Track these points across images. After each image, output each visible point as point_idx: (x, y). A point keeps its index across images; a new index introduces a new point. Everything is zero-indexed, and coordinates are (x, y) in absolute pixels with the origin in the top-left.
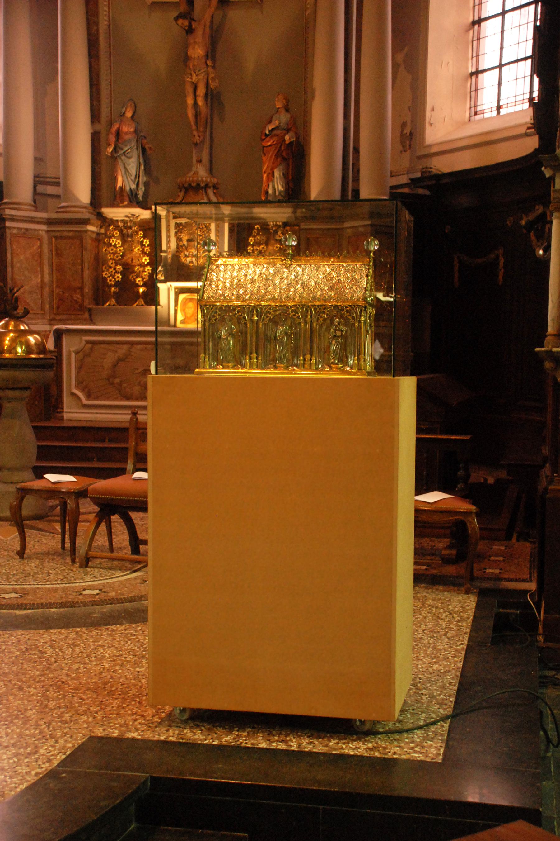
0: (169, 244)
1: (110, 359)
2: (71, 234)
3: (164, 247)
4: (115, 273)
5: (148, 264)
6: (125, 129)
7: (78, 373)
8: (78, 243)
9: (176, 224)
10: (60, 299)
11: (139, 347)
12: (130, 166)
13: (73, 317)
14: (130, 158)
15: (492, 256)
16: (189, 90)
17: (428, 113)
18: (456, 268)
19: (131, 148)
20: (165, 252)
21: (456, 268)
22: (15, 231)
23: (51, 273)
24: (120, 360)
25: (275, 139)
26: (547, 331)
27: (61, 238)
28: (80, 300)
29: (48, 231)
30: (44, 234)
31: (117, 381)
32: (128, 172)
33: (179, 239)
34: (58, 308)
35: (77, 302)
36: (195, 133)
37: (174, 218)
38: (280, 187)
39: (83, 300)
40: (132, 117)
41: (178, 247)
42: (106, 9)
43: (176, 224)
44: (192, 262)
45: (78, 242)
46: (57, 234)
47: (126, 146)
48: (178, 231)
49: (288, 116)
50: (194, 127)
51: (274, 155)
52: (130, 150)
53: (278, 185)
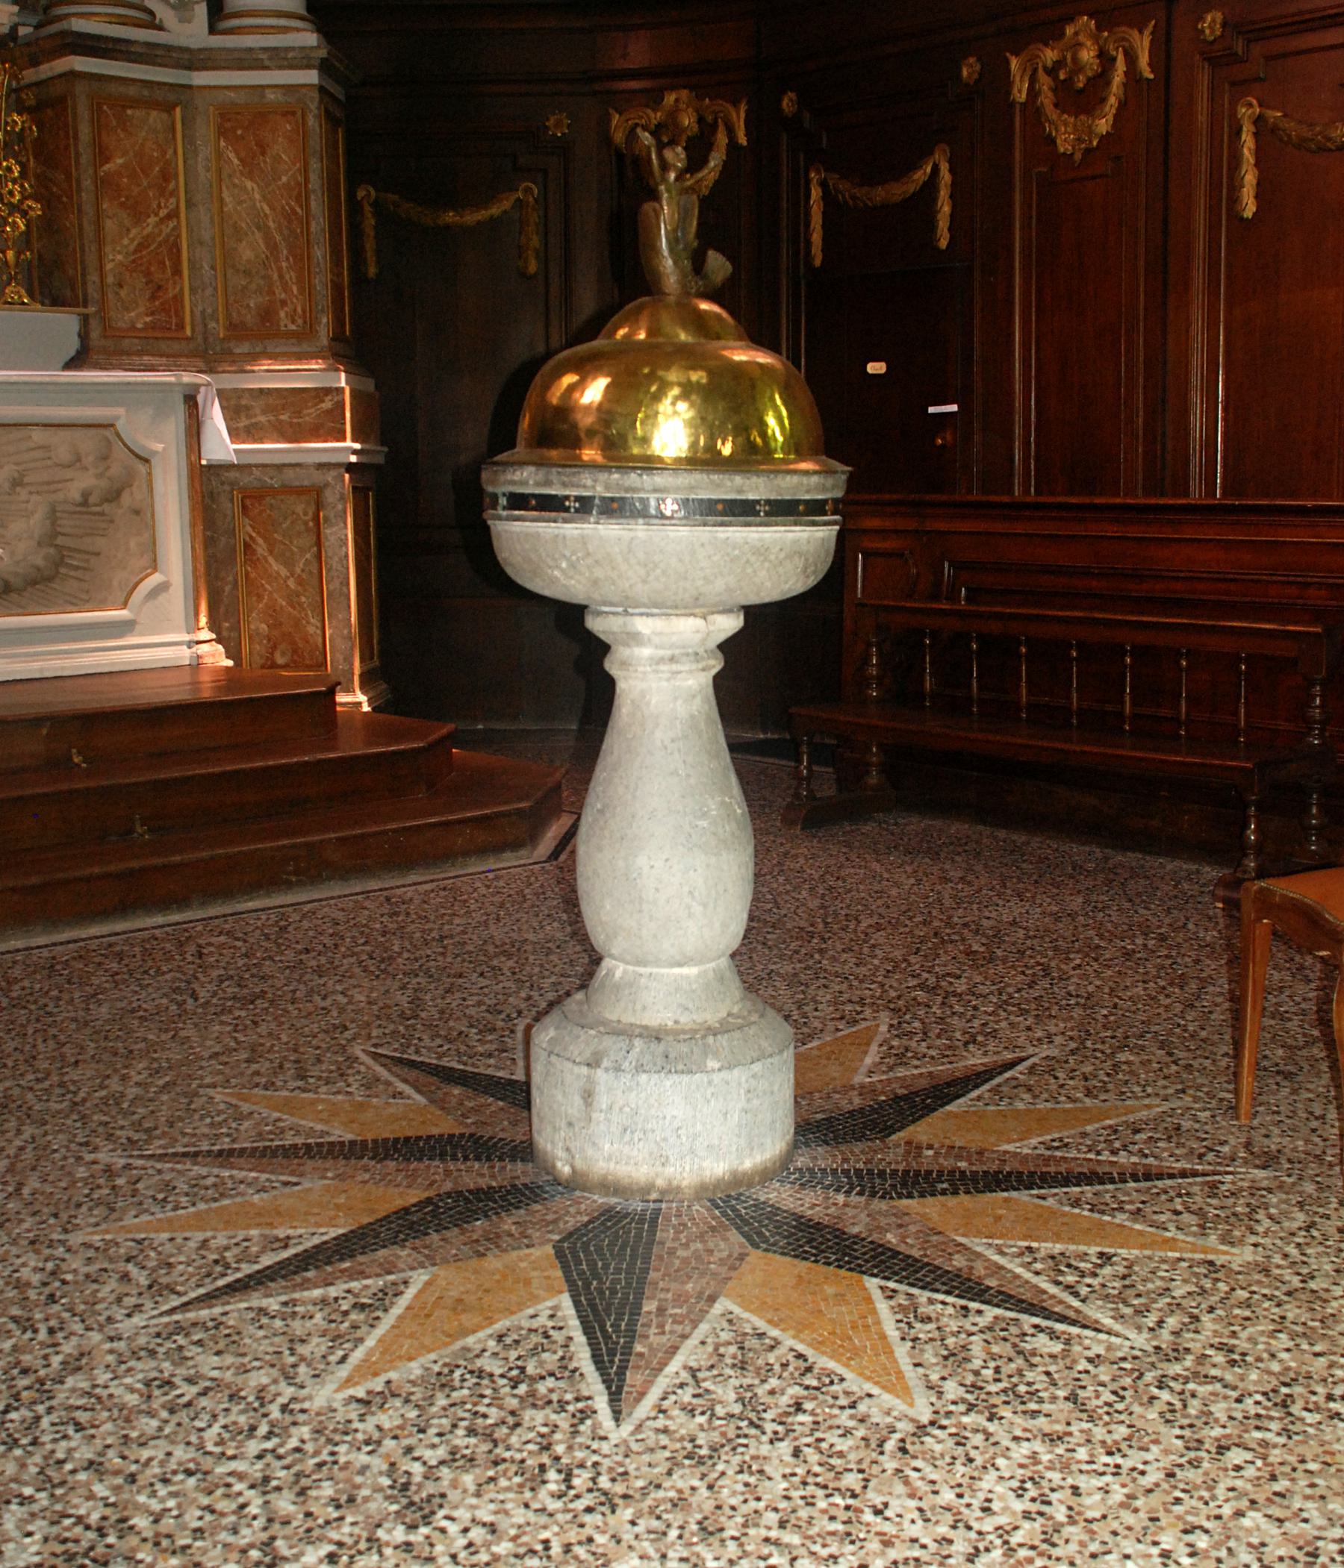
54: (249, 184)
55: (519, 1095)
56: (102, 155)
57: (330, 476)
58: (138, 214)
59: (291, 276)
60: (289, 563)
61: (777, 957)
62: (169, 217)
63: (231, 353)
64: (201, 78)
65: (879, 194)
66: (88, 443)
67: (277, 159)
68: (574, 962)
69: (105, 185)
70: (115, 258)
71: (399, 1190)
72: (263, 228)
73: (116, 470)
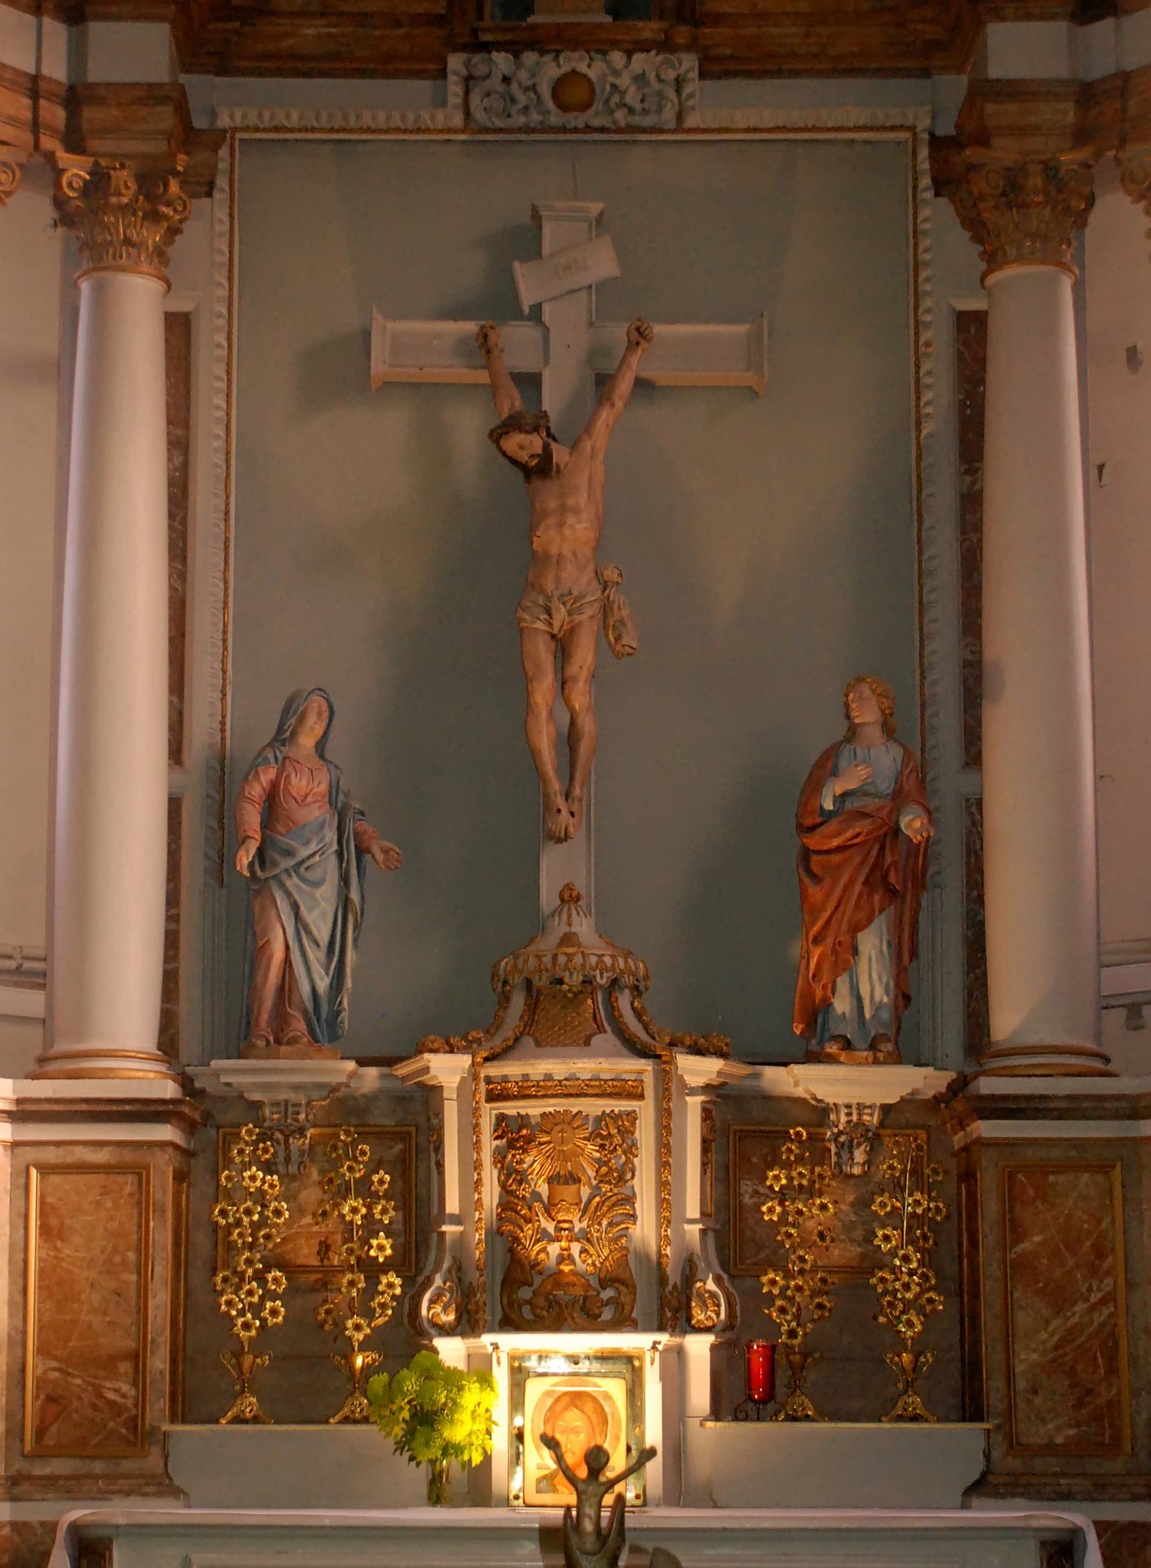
0: (466, 1191)
3: (452, 1205)
4: (262, 1298)
8: (128, 1189)
9: (501, 1118)
10: (51, 1399)
12: (315, 913)
13: (98, 1467)
14: (317, 884)
16: (542, 652)
19: (321, 851)
20: (456, 1220)
25: (862, 826)
26: (714, 1348)
28: (130, 1402)
32: (309, 933)
33: (512, 1178)
36: (560, 802)
37: (492, 1097)
38: (879, 993)
39: (141, 1401)
41: (509, 1203)
42: (220, 401)
43: (501, 1118)
45: (128, 1184)
47: (307, 843)
48: (511, 1145)
49: (897, 751)
50: (556, 786)
51: (862, 879)
52: (317, 858)
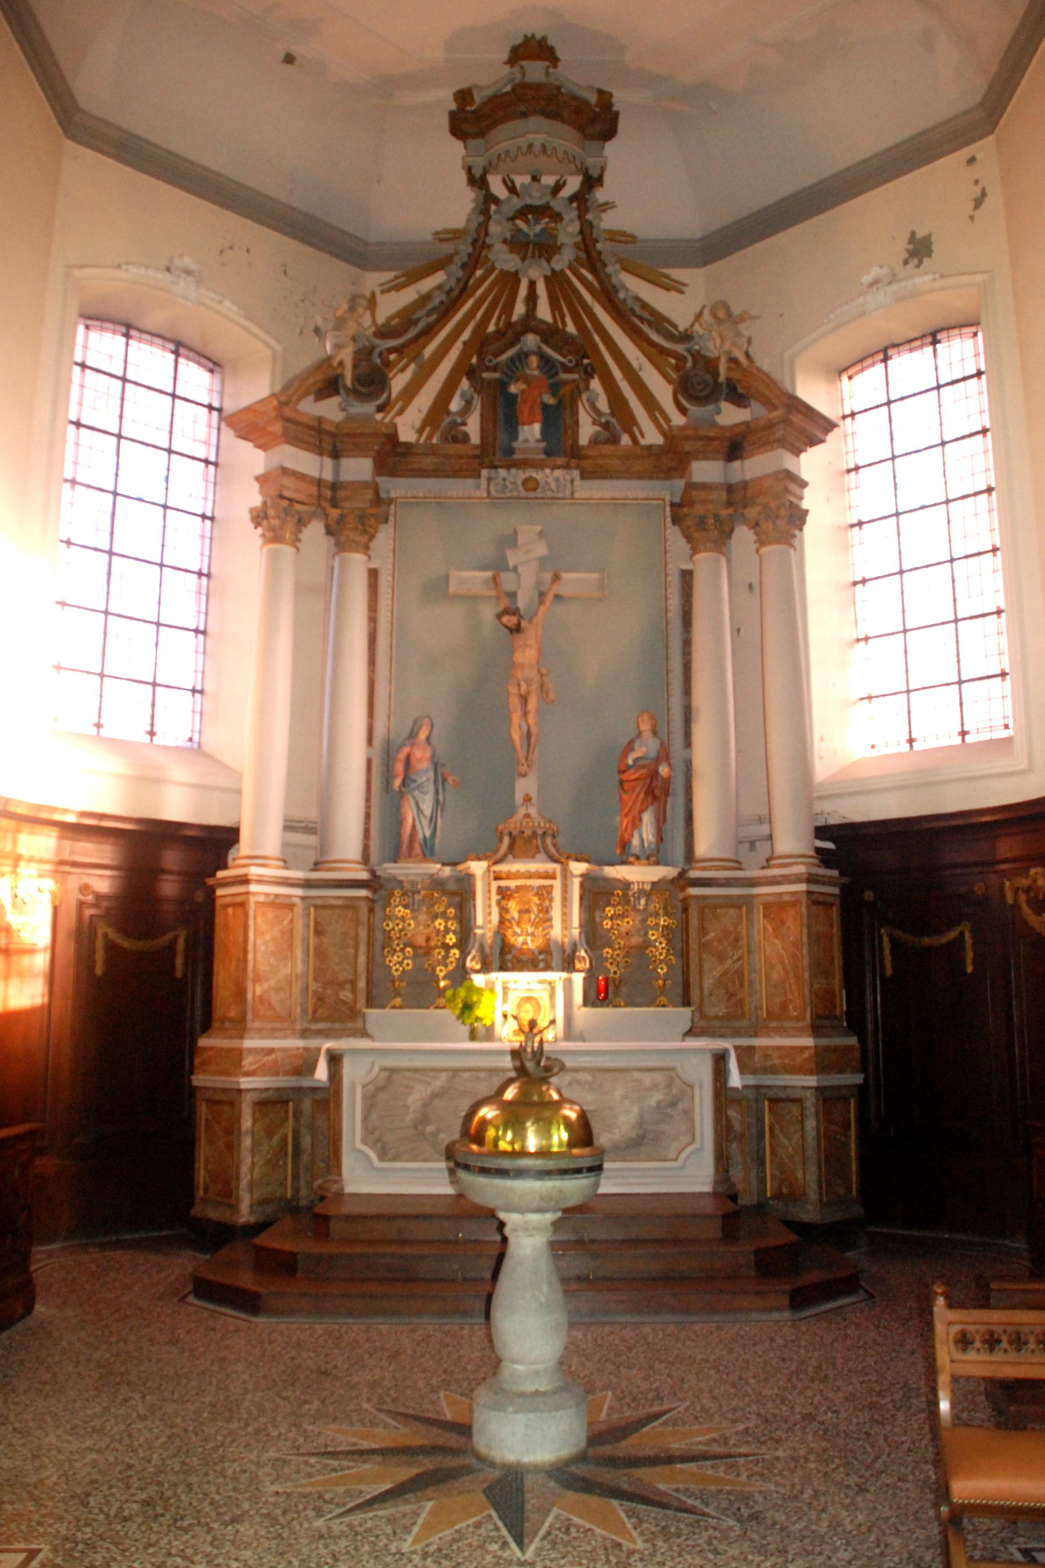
0: (485, 916)
1: (417, 1096)
2: (340, 902)
3: (480, 921)
5: (454, 946)
6: (418, 753)
7: (365, 1118)
9: (499, 887)
11: (466, 1075)
13: (337, 1026)
15: (952, 935)
16: (515, 702)
17: (817, 744)
18: (887, 951)
20: (481, 928)
21: (887, 951)
22: (261, 899)
23: (306, 960)
24: (435, 1095)
27: (323, 907)
29: (303, 898)
30: (297, 901)
31: (430, 1129)
33: (503, 910)
34: (315, 1012)
35: (344, 1002)
37: (496, 878)
38: (651, 837)
40: (428, 739)
41: (502, 921)
44: (525, 943)
46: (319, 902)
53: (646, 832)
54: (776, 941)
55: (465, 1429)
56: (703, 930)
57: (808, 1093)
58: (721, 958)
59: (794, 987)
60: (789, 1139)
61: (576, 1373)
62: (739, 959)
63: (767, 1027)
64: (757, 891)
65: (927, 941)
66: (659, 1077)
67: (788, 928)
68: (492, 1363)
69: (704, 947)
70: (708, 982)
71: (405, 1473)
72: (782, 963)
73: (675, 1091)
